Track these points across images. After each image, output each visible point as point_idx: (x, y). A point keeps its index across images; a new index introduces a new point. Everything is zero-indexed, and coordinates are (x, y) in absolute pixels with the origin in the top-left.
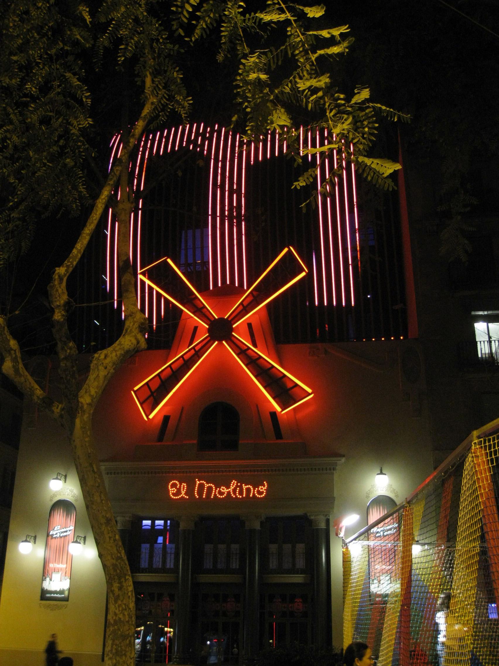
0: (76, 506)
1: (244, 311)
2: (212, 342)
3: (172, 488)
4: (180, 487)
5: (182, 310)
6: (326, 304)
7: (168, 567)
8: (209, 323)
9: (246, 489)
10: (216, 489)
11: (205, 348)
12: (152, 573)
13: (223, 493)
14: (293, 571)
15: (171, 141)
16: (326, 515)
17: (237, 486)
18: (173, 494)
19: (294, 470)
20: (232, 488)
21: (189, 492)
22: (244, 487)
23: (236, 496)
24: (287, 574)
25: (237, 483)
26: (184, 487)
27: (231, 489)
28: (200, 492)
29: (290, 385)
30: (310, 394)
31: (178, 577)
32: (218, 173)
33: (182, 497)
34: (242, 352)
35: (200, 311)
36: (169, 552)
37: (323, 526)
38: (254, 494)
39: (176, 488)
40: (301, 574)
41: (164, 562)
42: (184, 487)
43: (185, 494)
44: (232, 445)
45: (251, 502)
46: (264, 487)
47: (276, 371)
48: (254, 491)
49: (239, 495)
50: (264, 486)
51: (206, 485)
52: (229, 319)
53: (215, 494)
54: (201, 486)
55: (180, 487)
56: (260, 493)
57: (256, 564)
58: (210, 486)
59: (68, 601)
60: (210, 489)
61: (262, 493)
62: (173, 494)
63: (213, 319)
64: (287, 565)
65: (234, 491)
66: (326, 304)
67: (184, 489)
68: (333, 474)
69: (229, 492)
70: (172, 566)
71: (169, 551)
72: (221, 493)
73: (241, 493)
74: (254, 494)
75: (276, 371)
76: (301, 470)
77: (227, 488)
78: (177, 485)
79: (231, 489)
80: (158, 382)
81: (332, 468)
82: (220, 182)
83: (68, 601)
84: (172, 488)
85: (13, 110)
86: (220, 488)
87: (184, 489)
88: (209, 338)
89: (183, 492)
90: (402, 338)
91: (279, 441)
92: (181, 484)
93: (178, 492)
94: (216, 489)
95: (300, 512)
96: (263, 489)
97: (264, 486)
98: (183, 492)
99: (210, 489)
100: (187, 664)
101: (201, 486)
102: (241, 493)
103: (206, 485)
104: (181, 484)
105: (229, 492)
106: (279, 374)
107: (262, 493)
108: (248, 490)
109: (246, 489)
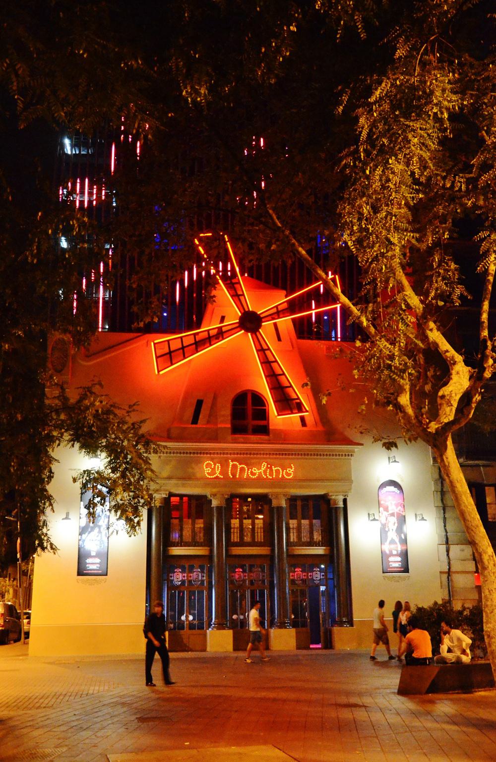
2: (239, 329)
3: (206, 468)
6: (313, 302)
7: (292, 540)
8: (243, 312)
9: (276, 470)
11: (230, 333)
13: (255, 474)
14: (311, 543)
16: (345, 496)
18: (208, 473)
22: (274, 469)
23: (267, 477)
24: (306, 546)
25: (267, 465)
26: (218, 467)
27: (262, 471)
30: (159, 372)
31: (211, 551)
35: (237, 296)
37: (341, 505)
39: (211, 468)
40: (322, 546)
42: (218, 467)
43: (220, 474)
45: (280, 482)
48: (283, 473)
49: (270, 475)
51: (239, 466)
54: (234, 466)
55: (215, 467)
56: (289, 475)
58: (243, 467)
59: (107, 575)
61: (290, 474)
62: (208, 473)
64: (248, 539)
65: (265, 472)
66: (313, 302)
67: (218, 469)
69: (261, 472)
71: (291, 526)
73: (271, 474)
74: (248, 475)
78: (211, 465)
79: (262, 471)
81: (350, 454)
83: (107, 575)
84: (206, 468)
85: (400, 136)
87: (218, 469)
88: (237, 325)
89: (218, 472)
90: (165, 314)
92: (215, 465)
93: (213, 472)
96: (291, 471)
99: (242, 469)
100: (10, 644)
101: (234, 466)
102: (271, 474)
103: (239, 466)
104: (215, 465)
106: (214, 342)
107: (290, 474)
109: (276, 470)
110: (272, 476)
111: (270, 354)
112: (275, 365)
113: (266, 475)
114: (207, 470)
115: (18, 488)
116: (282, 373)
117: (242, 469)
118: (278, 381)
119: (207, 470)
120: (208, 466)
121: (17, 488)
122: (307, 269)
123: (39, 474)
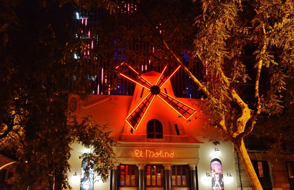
0: (221, 161)
1: (143, 83)
4: (140, 152)
5: (136, 83)
7: (173, 185)
10: (169, 154)
12: (132, 187)
19: (180, 147)
20: (161, 153)
21: (144, 155)
22: (165, 153)
23: (162, 157)
26: (141, 152)
27: (160, 154)
33: (141, 156)
34: (148, 101)
36: (173, 179)
37: (194, 169)
38: (169, 156)
39: (138, 153)
41: (156, 183)
42: (141, 152)
44: (160, 137)
46: (173, 153)
50: (173, 153)
55: (140, 152)
56: (172, 156)
57: (166, 184)
60: (152, 154)
61: (172, 156)
63: (159, 86)
64: (154, 184)
65: (162, 155)
68: (198, 149)
70: (175, 184)
72: (156, 155)
74: (169, 156)
76: (187, 147)
79: (160, 154)
81: (198, 147)
82: (88, 33)
91: (179, 136)
92: (140, 151)
93: (139, 155)
94: (169, 154)
95: (186, 164)
96: (173, 154)
99: (152, 154)
104: (140, 151)
107: (172, 156)
112: (173, 101)
119: (137, 154)
120: (137, 152)
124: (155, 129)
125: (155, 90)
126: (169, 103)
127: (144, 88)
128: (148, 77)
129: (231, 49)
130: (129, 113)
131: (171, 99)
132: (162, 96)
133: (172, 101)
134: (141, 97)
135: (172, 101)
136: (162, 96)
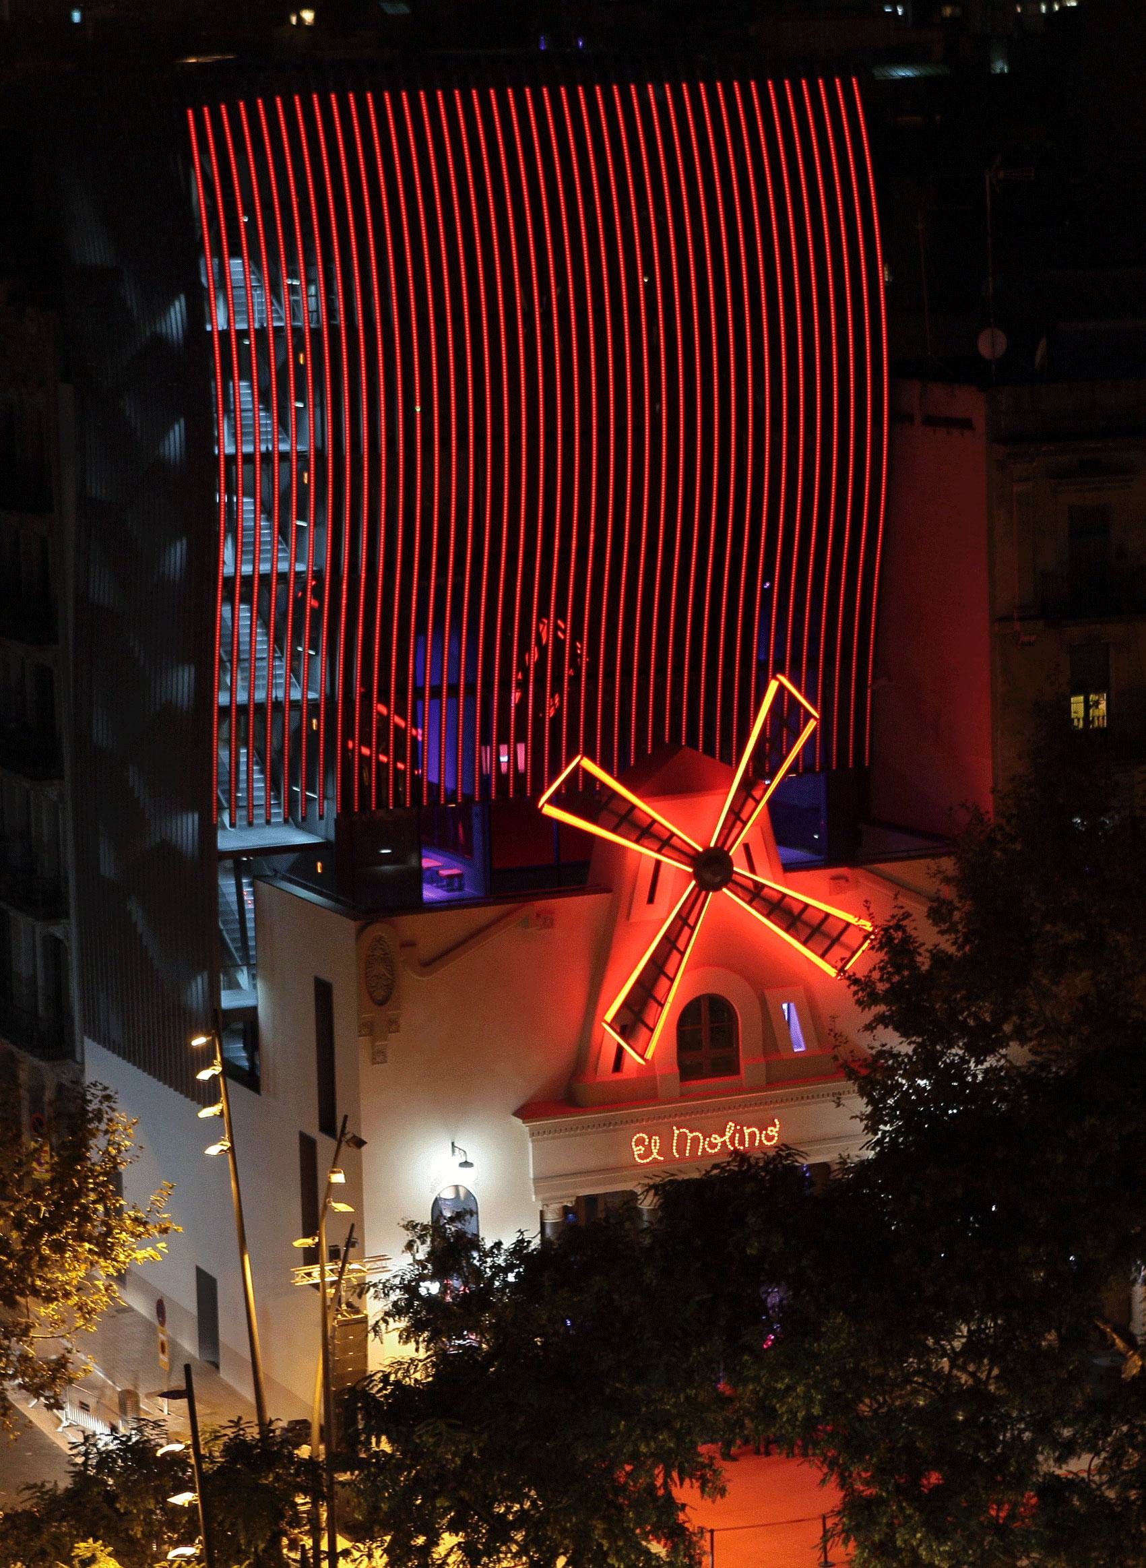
13: (715, 1145)
15: (192, 124)
17: (735, 1131)
18: (639, 1155)
20: (728, 1134)
22: (747, 1131)
27: (726, 1138)
28: (681, 1150)
29: (797, 909)
32: (595, 532)
47: (771, 892)
52: (735, 877)
53: (704, 1149)
54: (683, 1137)
56: (769, 1138)
62: (639, 1155)
69: (725, 1142)
73: (742, 1142)
74: (704, 1149)
75: (771, 892)
77: (722, 1137)
78: (644, 1140)
79: (726, 1138)
80: (659, 994)
86: (710, 1137)
92: (650, 1139)
93: (648, 1152)
96: (773, 1131)
97: (775, 1126)
98: (655, 1151)
99: (695, 1140)
101: (683, 1137)
103: (690, 1135)
104: (650, 1139)
105: (725, 1142)
106: (775, 894)
108: (752, 1135)
110: (744, 1145)
111: (627, 904)
112: (675, 956)
113: (733, 1144)
114: (638, 1150)
115: (1050, 8)
116: (671, 976)
117: (752, 1135)
118: (655, 981)
119: (638, 1150)
120: (640, 1142)
121: (1044, 8)
122: (268, 409)
123: (256, 1446)
124: (710, 1038)
125: (712, 868)
126: (767, 916)
127: (658, 863)
128: (767, 818)
129: (1035, 1452)
130: (612, 975)
131: (681, 944)
132: (740, 888)
133: (675, 952)
134: (651, 900)
135: (675, 952)
136: (688, 906)
